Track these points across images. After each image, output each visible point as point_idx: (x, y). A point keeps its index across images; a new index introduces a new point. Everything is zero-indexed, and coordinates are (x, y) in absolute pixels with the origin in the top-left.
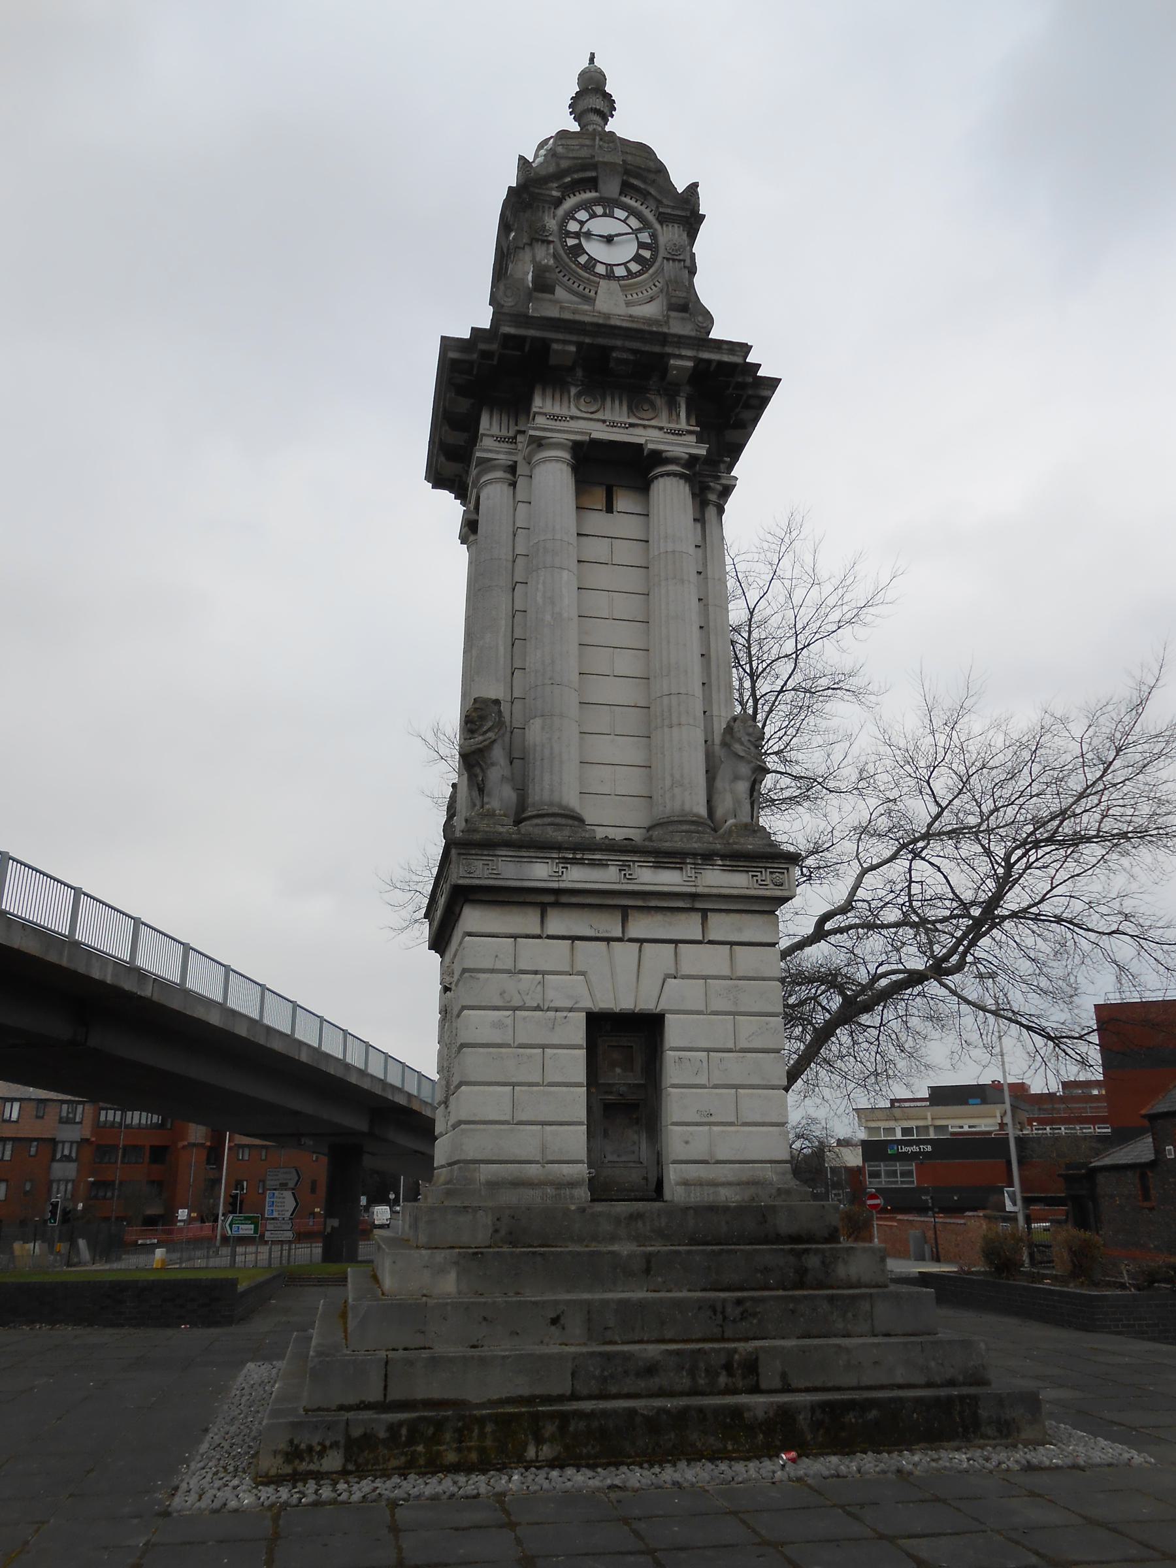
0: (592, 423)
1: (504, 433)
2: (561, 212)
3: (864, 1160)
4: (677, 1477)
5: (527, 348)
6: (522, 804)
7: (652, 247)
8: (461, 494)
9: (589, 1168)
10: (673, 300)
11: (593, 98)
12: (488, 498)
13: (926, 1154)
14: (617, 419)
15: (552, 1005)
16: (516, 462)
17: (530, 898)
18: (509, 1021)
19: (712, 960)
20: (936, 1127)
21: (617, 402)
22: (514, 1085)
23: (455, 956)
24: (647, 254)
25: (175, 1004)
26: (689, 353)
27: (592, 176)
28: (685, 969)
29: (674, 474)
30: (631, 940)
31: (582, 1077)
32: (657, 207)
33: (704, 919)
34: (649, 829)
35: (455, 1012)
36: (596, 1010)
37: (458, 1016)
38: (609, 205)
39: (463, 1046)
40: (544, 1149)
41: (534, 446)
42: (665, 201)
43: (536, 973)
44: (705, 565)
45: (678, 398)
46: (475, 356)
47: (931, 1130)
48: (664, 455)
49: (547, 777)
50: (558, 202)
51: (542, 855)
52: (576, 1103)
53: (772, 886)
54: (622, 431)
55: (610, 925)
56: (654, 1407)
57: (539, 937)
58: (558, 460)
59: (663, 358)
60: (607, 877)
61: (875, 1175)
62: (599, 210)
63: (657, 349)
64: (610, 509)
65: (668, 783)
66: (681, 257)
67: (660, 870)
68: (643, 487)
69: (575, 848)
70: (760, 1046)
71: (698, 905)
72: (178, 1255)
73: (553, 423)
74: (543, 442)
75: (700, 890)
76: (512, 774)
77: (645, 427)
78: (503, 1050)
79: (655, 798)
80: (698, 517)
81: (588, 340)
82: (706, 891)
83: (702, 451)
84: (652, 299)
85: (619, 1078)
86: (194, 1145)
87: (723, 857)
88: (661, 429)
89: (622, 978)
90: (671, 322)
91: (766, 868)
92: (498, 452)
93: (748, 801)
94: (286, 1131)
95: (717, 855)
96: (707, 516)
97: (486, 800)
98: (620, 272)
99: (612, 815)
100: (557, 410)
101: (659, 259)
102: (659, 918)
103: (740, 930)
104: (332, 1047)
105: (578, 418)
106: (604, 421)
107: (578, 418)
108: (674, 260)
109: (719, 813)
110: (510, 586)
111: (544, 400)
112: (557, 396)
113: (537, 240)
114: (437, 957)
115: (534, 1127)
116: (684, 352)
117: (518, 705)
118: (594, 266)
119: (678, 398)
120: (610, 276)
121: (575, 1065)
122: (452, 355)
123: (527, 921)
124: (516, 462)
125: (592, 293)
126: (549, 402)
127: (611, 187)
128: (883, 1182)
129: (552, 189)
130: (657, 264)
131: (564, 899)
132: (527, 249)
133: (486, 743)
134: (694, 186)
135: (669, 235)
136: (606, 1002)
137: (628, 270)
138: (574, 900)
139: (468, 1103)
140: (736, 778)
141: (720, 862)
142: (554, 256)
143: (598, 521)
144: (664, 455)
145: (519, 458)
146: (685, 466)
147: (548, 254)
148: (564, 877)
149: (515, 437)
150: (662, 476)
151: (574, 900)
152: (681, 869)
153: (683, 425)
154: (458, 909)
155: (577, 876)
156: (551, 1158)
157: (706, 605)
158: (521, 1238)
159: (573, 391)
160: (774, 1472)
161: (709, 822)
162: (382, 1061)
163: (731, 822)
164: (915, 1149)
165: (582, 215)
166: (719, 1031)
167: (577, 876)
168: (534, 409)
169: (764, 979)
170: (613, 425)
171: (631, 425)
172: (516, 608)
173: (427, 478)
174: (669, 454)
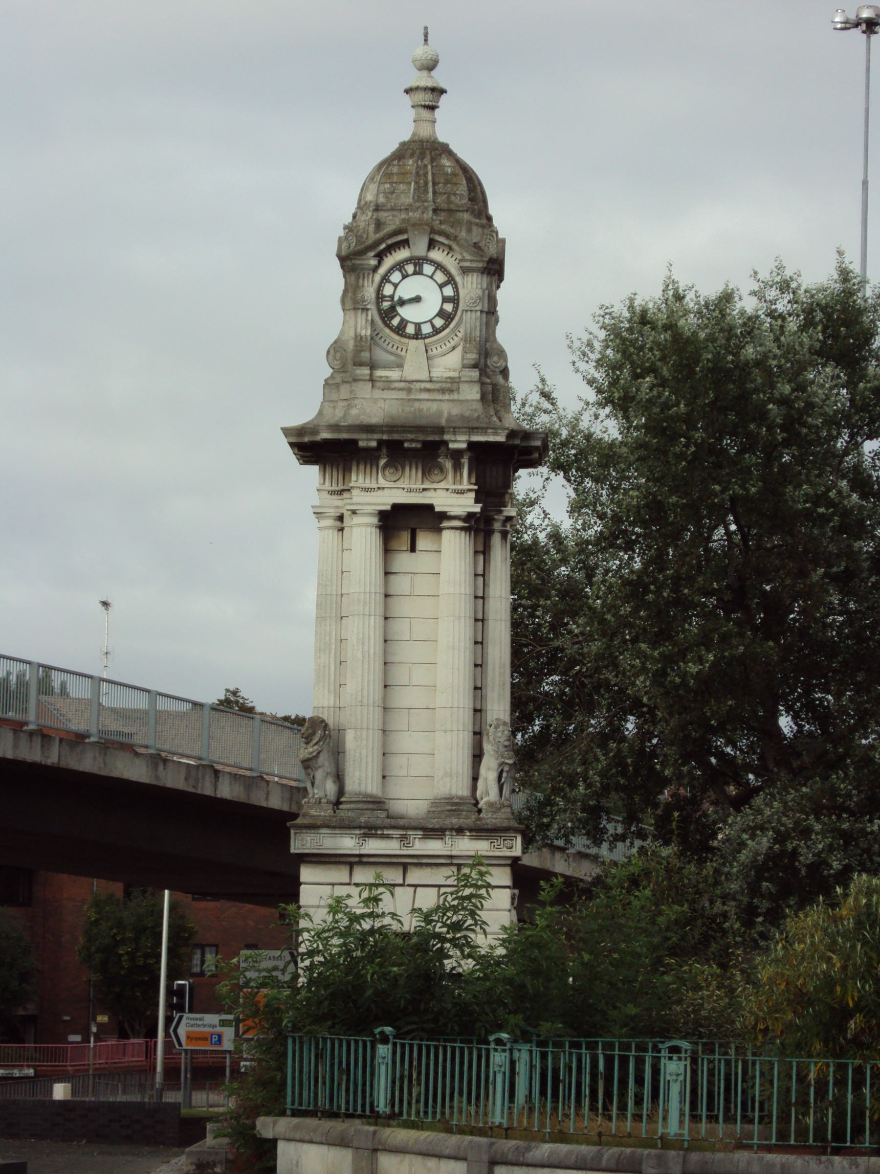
1: (334, 488)
7: (454, 300)
10: (465, 362)
17: (342, 860)
24: (449, 307)
29: (456, 528)
30: (409, 885)
45: (462, 460)
49: (357, 774)
50: (375, 269)
53: (505, 849)
54: (417, 494)
57: (349, 884)
60: (390, 847)
75: (454, 853)
82: (458, 853)
83: (477, 509)
84: (454, 348)
87: (471, 830)
90: (463, 387)
91: (501, 837)
98: (426, 329)
99: (412, 797)
100: (368, 484)
102: (428, 871)
105: (383, 488)
108: (471, 311)
112: (368, 470)
119: (462, 460)
120: (418, 335)
124: (343, 514)
127: (419, 248)
130: (457, 318)
131: (365, 860)
133: (314, 754)
137: (433, 326)
138: (371, 860)
141: (468, 834)
147: (367, 320)
151: (371, 860)
155: (374, 846)
159: (382, 462)
163: (485, 799)
167: (374, 846)
169: (498, 910)
170: (410, 490)
171: (424, 490)
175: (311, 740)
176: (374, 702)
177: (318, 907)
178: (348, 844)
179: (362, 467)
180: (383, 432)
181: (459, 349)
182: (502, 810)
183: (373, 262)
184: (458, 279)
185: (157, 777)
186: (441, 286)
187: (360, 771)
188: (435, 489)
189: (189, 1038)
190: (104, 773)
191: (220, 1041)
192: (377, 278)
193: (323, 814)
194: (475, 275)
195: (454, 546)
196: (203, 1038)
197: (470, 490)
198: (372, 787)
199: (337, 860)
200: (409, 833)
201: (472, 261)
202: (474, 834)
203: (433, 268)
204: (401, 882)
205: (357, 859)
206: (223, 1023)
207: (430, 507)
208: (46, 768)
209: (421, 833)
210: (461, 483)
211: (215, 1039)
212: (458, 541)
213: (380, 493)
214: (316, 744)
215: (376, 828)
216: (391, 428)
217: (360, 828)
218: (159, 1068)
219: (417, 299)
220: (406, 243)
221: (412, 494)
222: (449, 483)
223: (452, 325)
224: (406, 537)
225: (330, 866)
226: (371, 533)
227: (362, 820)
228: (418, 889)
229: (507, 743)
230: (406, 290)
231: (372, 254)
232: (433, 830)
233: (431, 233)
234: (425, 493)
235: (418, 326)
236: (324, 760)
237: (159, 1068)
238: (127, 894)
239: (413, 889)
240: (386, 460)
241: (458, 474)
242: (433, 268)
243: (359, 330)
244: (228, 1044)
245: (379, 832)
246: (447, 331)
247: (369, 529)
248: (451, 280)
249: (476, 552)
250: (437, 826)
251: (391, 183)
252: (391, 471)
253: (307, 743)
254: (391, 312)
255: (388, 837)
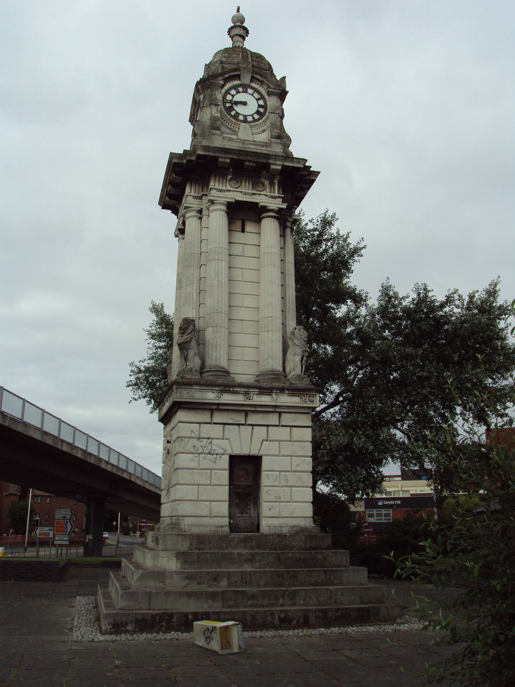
0: (236, 193)
1: (197, 195)
2: (223, 91)
3: (366, 508)
4: (262, 634)
5: (208, 159)
6: (203, 366)
7: (265, 107)
8: (175, 212)
9: (229, 519)
10: (273, 134)
11: (239, 29)
12: (190, 224)
13: (397, 505)
14: (247, 191)
15: (215, 452)
16: (202, 209)
18: (197, 459)
19: (283, 433)
20: (403, 491)
21: (247, 183)
22: (199, 485)
23: (173, 428)
24: (262, 110)
25: (20, 429)
26: (280, 163)
27: (238, 72)
28: (271, 437)
30: (249, 425)
31: (227, 482)
32: (267, 88)
33: (280, 416)
34: (257, 376)
35: (173, 453)
36: (234, 454)
37: (175, 455)
38: (245, 87)
39: (177, 469)
40: (210, 510)
41: (210, 203)
42: (271, 86)
43: (208, 438)
44: (285, 256)
46: (185, 161)
47: (401, 492)
48: (268, 208)
49: (214, 354)
50: (223, 86)
51: (212, 389)
52: (224, 492)
53: (309, 402)
54: (249, 196)
55: (240, 418)
56: (254, 611)
57: (210, 423)
58: (220, 210)
59: (268, 165)
60: (238, 399)
61: (371, 516)
62: (241, 89)
63: (265, 161)
64: (243, 231)
65: (266, 356)
66: (277, 112)
67: (262, 396)
68: (259, 221)
69: (225, 386)
70: (302, 469)
71: (278, 410)
72: (10, 551)
73: (219, 193)
74: (215, 202)
75: (278, 404)
76: (199, 351)
77: (259, 194)
78: (195, 471)
79: (260, 362)
80: (282, 234)
81: (235, 157)
83: (284, 206)
84: (264, 131)
85: (243, 482)
86: (12, 494)
87: (288, 390)
88: (266, 195)
89: (243, 440)
90: (272, 145)
91: (307, 394)
92: (194, 204)
93: (300, 364)
94: (61, 489)
95: (286, 389)
96: (286, 233)
97: (188, 364)
98: (250, 119)
99: (244, 372)
100: (221, 187)
101: (267, 113)
102: (261, 415)
103: (295, 421)
104: (93, 450)
105: (230, 191)
106: (241, 192)
107: (230, 191)
108: (274, 113)
109: (288, 369)
110: (199, 266)
111: (215, 182)
112: (221, 180)
113: (213, 104)
114: (162, 425)
115: (206, 503)
116: (277, 162)
117: (202, 320)
118: (238, 116)
120: (245, 121)
121: (224, 477)
122: (175, 161)
123: (205, 417)
124: (202, 209)
125: (237, 129)
126: (217, 184)
127: (246, 79)
128: (372, 520)
129: (219, 80)
130: (266, 115)
131: (221, 407)
132: (208, 107)
133: (189, 339)
134: (284, 78)
135: (272, 101)
136: (237, 451)
137: (253, 118)
138: (225, 408)
139: (178, 492)
140: (295, 354)
141: (287, 392)
142: (220, 112)
143: (238, 237)
144: (268, 208)
145: (203, 207)
146: (276, 213)
147: (217, 111)
148: (221, 398)
149: (202, 197)
150: (267, 217)
151: (225, 408)
152: (271, 395)
153: (276, 194)
154: (175, 410)
155: (227, 398)
156: (213, 515)
157: (285, 262)
158: (200, 549)
159: (229, 177)
160: (299, 633)
161: (283, 374)
162: (126, 461)
163: (292, 373)
164: (392, 502)
165: (233, 92)
166: (285, 463)
167: (227, 398)
168: (210, 187)
170: (245, 194)
171: (254, 194)
172: (201, 276)
173: (160, 204)
174: (270, 208)
175: (186, 331)
176: (225, 312)
177: (190, 438)
178: (211, 396)
179: (217, 179)
180: (234, 154)
181: (269, 130)
182: (305, 380)
183: (222, 82)
184: (266, 97)
185: (43, 439)
186: (257, 100)
187: (216, 352)
188: (259, 194)
189: (40, 534)
190: (25, 433)
191: (48, 535)
192: (223, 91)
193: (193, 377)
194: (275, 97)
195: (270, 227)
196: (44, 534)
197: (279, 197)
198: (223, 363)
199: (203, 407)
200: (250, 390)
201: (274, 89)
202: (291, 392)
203: (253, 91)
204: (244, 422)
205: (215, 407)
206: (50, 530)
207: (257, 204)
208: (3, 426)
209: (258, 391)
210: (274, 192)
211: (47, 534)
212: (272, 224)
213: (228, 193)
214: (189, 334)
215: (230, 386)
216: (240, 152)
217: (219, 386)
218: (26, 542)
219: (245, 104)
220: (238, 77)
221: (247, 196)
222: (267, 192)
223: (264, 119)
224: (239, 224)
225: (196, 411)
226: (223, 215)
227: (220, 381)
228: (255, 427)
229: (306, 339)
230: (239, 98)
231: (221, 78)
232: (265, 389)
233: (252, 73)
234: (253, 196)
235: (245, 116)
236: (193, 343)
237: (26, 542)
238: (19, 500)
239: (251, 427)
240: (231, 176)
241: (272, 188)
242: (253, 91)
243: (213, 113)
244: (51, 536)
245: (231, 389)
246: (261, 121)
247: (221, 212)
248: (262, 97)
249: (281, 236)
250: (268, 386)
251: (229, 54)
252: (234, 182)
253: (183, 334)
254: (231, 109)
255: (237, 393)
